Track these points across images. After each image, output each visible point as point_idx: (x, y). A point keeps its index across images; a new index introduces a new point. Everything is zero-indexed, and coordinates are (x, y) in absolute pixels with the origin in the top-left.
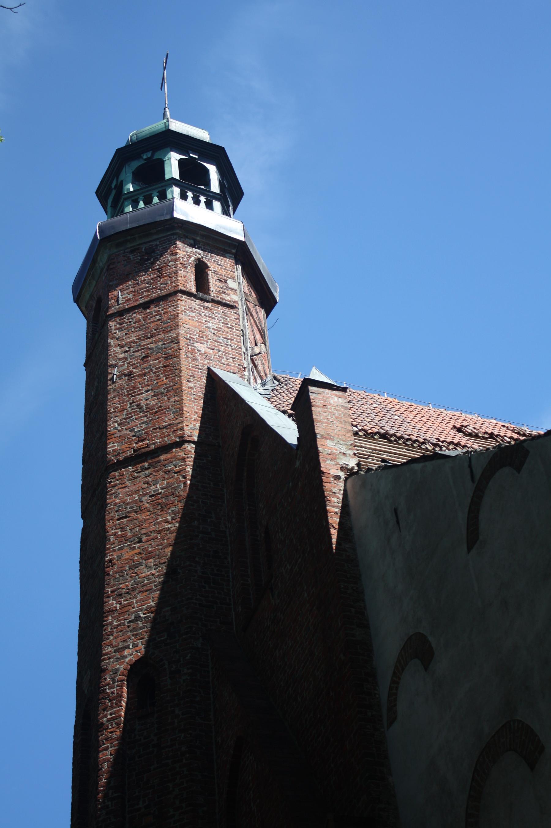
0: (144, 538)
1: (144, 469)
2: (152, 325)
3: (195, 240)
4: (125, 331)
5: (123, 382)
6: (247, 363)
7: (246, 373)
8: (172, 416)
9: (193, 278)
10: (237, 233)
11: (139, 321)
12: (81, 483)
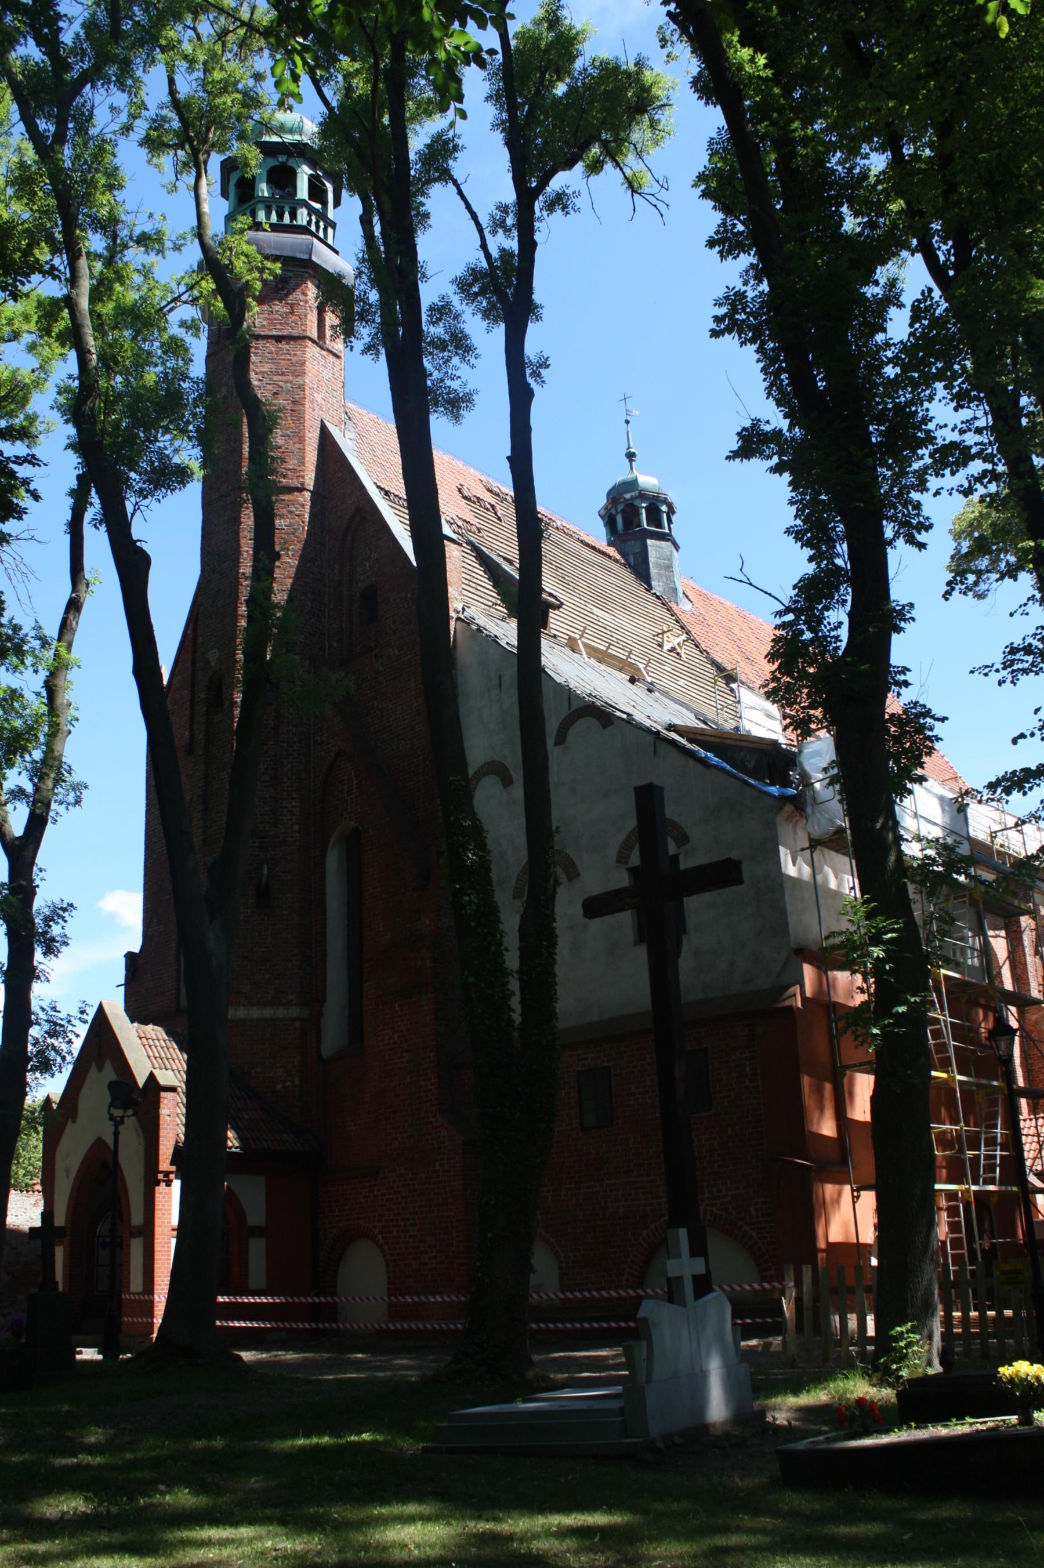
2: (283, 362)
11: (272, 353)
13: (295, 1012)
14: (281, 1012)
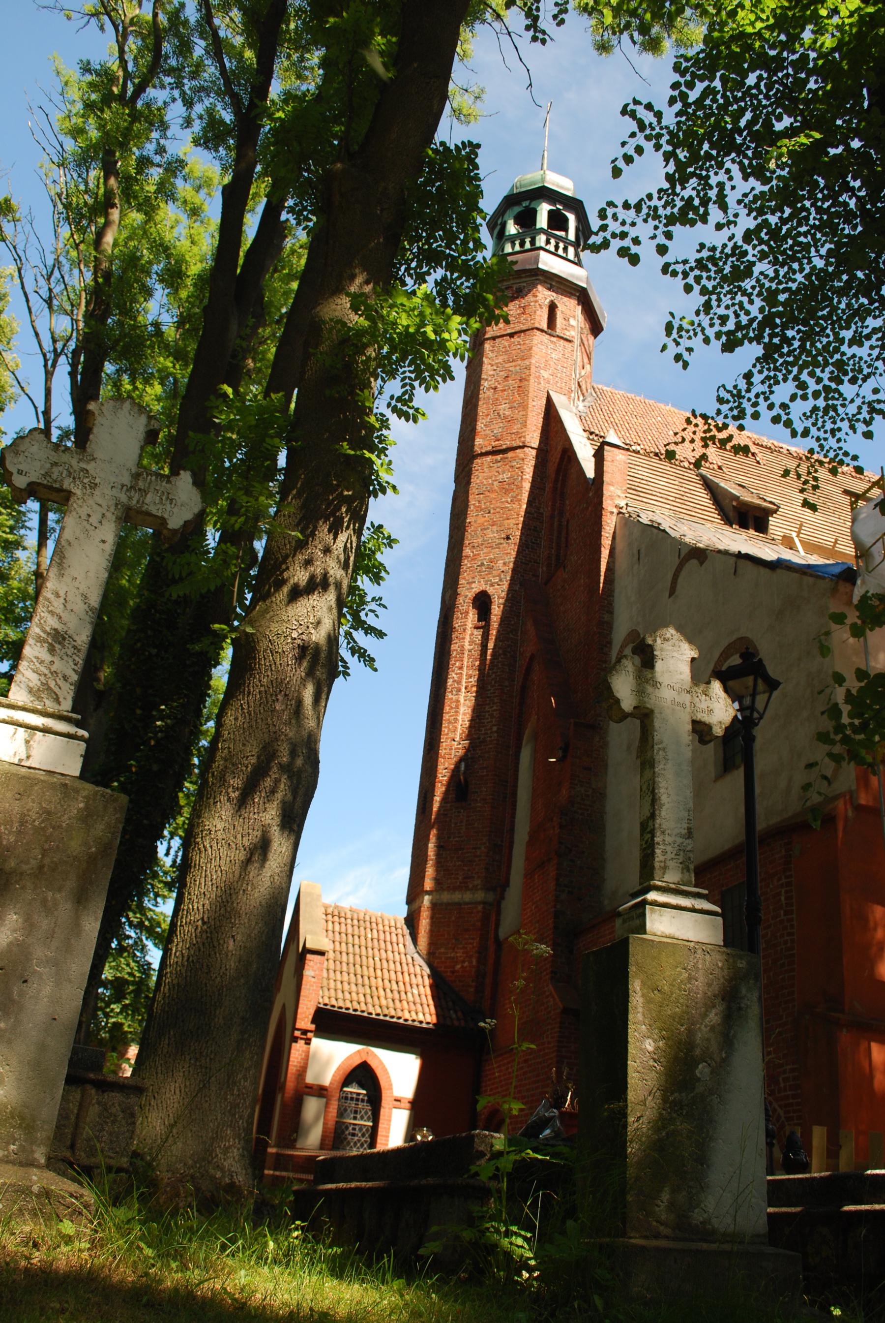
0: (492, 511)
1: (497, 462)
2: (513, 352)
3: (551, 285)
4: (495, 354)
5: (490, 393)
6: (574, 386)
7: (573, 395)
8: (519, 426)
9: (546, 316)
10: (581, 281)
12: (454, 488)
13: (480, 896)
14: (468, 897)
